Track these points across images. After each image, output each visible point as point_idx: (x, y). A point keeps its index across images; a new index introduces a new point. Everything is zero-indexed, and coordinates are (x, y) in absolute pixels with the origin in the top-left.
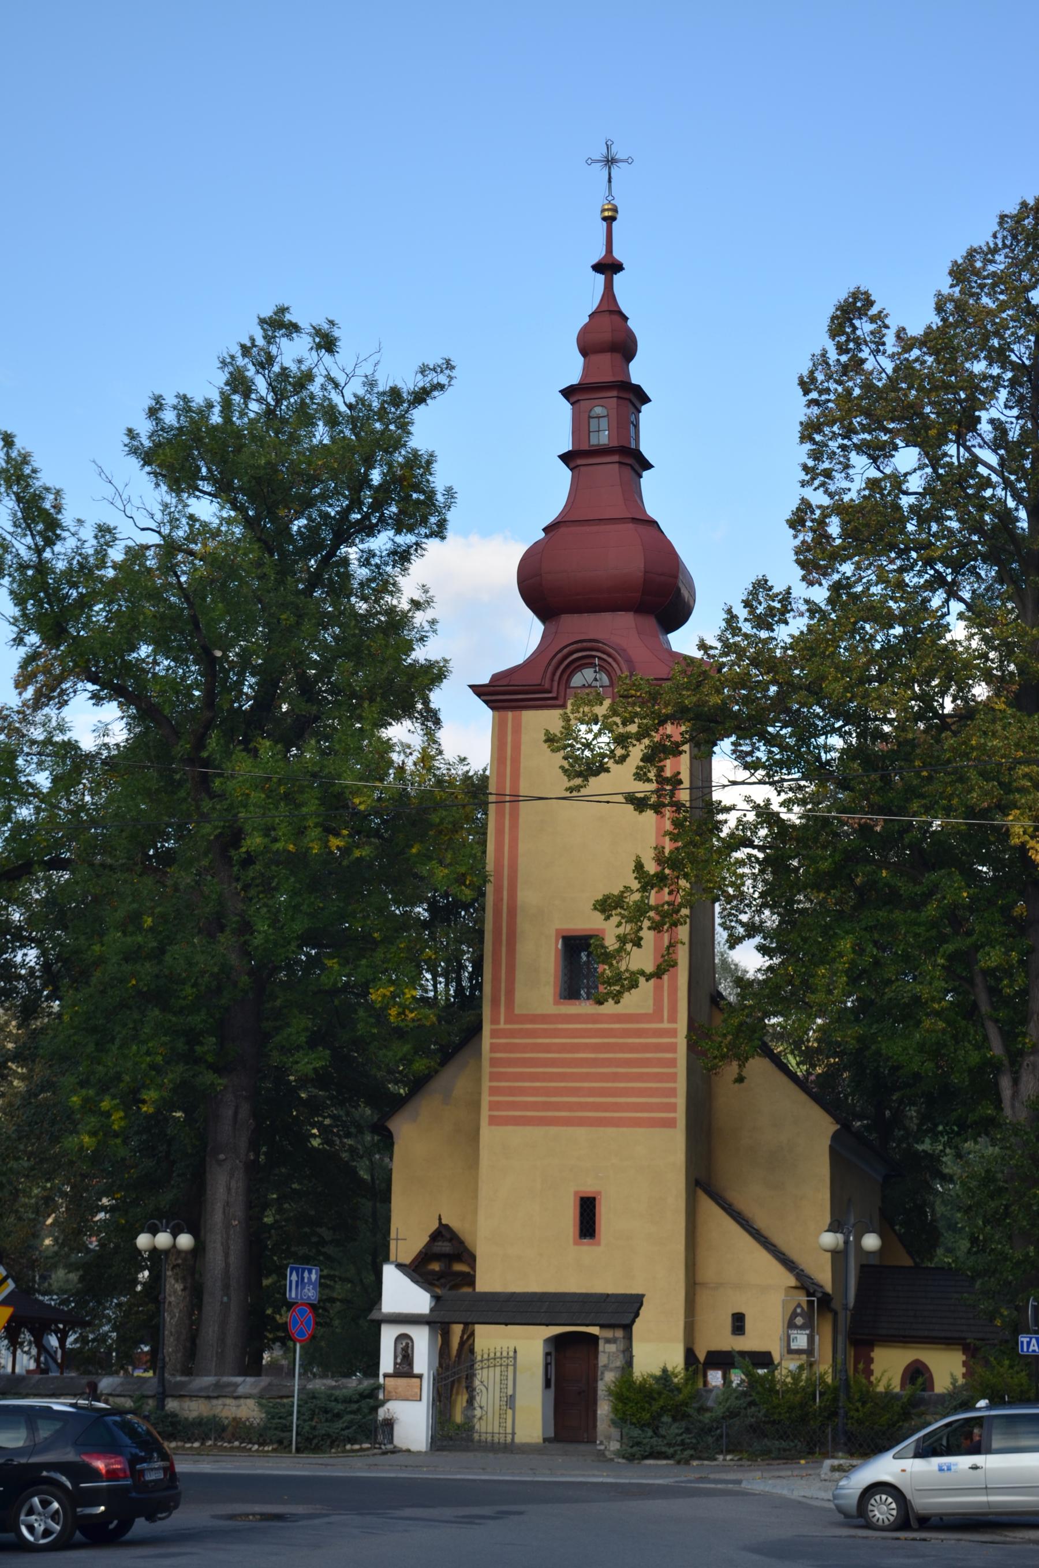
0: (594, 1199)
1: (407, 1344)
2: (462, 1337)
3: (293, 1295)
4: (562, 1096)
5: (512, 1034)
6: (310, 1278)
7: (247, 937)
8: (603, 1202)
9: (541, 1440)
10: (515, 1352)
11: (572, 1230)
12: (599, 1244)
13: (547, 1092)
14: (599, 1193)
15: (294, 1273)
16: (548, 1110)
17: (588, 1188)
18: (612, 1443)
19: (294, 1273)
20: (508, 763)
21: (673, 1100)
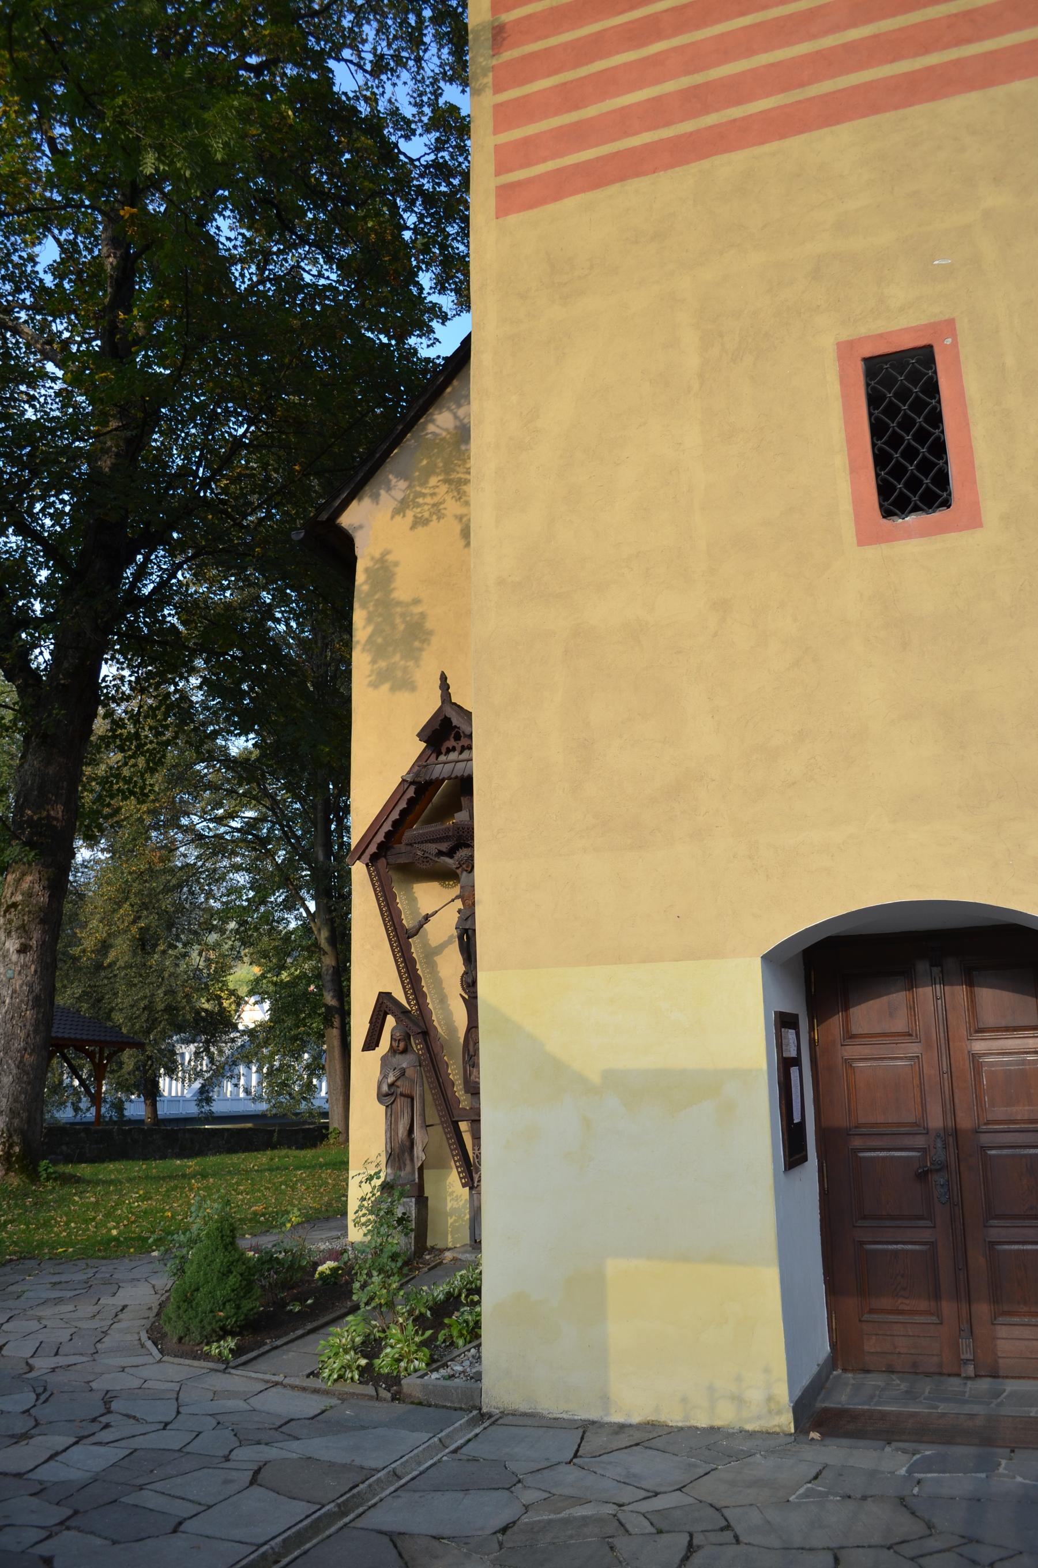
0: (925, 356)
4: (751, 52)
7: (411, 663)
8: (967, 351)
9: (786, 1421)
11: (844, 487)
14: (949, 326)
16: (707, 109)
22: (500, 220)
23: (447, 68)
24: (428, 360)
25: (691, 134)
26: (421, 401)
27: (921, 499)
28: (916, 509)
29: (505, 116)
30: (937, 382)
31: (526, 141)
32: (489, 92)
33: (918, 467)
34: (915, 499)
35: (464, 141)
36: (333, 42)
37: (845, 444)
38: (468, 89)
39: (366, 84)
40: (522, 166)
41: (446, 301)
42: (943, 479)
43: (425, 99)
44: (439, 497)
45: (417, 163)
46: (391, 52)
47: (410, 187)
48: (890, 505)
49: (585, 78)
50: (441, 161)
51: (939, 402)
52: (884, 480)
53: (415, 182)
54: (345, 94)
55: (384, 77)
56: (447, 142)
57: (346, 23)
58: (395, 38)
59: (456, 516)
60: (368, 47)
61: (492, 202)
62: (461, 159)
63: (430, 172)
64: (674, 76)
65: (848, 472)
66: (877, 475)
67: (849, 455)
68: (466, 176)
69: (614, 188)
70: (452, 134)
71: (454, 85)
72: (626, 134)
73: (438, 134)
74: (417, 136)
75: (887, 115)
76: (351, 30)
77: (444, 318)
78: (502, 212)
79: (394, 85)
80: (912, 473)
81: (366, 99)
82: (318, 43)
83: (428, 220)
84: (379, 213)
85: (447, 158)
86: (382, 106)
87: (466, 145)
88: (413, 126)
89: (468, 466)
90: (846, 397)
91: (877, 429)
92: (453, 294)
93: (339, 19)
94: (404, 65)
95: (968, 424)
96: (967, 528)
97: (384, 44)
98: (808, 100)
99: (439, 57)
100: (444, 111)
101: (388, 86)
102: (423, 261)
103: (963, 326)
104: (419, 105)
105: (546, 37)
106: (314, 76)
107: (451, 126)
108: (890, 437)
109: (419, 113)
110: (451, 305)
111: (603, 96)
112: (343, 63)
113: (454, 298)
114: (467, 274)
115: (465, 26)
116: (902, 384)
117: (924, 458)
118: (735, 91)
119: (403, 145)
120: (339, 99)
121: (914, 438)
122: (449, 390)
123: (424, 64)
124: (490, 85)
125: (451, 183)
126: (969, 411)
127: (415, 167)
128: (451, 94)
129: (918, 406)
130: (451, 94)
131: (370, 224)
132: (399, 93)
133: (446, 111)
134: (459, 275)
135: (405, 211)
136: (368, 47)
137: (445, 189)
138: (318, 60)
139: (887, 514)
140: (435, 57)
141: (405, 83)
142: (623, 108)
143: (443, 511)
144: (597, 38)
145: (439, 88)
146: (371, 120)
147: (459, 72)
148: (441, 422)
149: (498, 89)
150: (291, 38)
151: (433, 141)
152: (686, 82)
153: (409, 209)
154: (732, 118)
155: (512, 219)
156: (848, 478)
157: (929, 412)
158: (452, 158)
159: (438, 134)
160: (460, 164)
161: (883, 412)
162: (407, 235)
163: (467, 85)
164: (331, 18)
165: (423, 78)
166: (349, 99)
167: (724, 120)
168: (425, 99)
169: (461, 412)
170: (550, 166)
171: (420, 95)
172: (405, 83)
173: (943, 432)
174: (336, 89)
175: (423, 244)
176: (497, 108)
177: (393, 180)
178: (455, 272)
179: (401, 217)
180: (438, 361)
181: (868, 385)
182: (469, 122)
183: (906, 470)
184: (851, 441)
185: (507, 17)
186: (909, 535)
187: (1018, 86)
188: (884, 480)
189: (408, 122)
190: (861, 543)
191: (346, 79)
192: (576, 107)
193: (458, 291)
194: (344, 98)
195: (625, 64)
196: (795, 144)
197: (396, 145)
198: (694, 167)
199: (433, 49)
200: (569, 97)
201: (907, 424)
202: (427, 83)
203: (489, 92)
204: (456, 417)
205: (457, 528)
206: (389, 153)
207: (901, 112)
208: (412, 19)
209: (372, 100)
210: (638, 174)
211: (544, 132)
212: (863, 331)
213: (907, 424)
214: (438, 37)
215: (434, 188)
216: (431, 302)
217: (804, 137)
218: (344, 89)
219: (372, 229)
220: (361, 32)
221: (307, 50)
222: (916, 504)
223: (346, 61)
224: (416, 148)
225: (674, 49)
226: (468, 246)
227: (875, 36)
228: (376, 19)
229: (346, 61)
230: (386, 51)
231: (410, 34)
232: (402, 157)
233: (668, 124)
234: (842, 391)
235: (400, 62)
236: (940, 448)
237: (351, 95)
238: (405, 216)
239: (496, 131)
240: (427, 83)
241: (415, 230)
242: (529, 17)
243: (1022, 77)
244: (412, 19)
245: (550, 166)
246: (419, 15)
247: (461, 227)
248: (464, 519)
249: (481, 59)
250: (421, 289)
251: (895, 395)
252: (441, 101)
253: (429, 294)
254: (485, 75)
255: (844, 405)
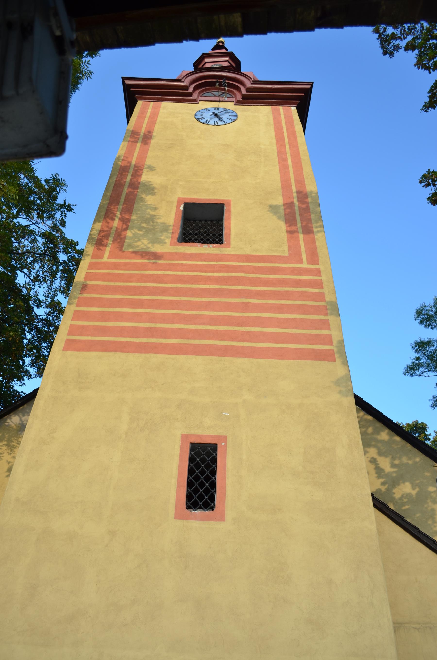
0: (214, 448)
4: (173, 322)
5: (116, 266)
13: (152, 318)
14: (224, 438)
16: (152, 337)
17: (205, 432)
21: (325, 332)
22: (64, 352)
23: (62, 288)
24: (17, 391)
25: (145, 343)
26: (8, 409)
27: (203, 504)
28: (200, 508)
29: (77, 315)
30: (217, 458)
31: (82, 327)
32: (74, 305)
33: (204, 491)
34: (201, 503)
35: (60, 315)
36: (22, 265)
37: (177, 475)
38: (68, 298)
39: (29, 283)
40: (78, 335)
41: (33, 371)
42: (212, 498)
43: (50, 295)
44: (2, 450)
45: (39, 317)
46: (43, 275)
47: (33, 325)
48: (191, 504)
49: (112, 312)
50: (48, 319)
51: (216, 466)
52: (190, 493)
53: (35, 323)
54: (19, 284)
55: (37, 283)
56: (53, 313)
57: (29, 260)
58: (46, 272)
59: (7, 461)
60: (34, 271)
61: (63, 344)
62: (56, 321)
63: (43, 322)
64: (144, 322)
65: (176, 487)
66: (187, 490)
67: (178, 480)
68: (56, 329)
69: (111, 354)
70: (56, 311)
71: (63, 295)
72: (122, 336)
73: (50, 310)
74: (42, 308)
75: (216, 357)
76: (30, 263)
77: (30, 377)
78: (65, 349)
79: (39, 287)
80: (201, 493)
81: (27, 288)
82: (16, 264)
83: (36, 339)
84: (16, 331)
85: (51, 319)
86: (32, 293)
87: (60, 317)
88: (42, 304)
89: (20, 439)
90: (181, 456)
91: (191, 472)
92: (36, 369)
93: (27, 258)
94: (46, 282)
95: (225, 478)
96: (219, 520)
97: (41, 272)
98: (189, 344)
99: (60, 284)
100: (55, 303)
101: (37, 287)
102: (28, 354)
103: (229, 439)
104: (47, 297)
105: (101, 294)
106: (10, 274)
107: (57, 309)
108: (195, 476)
109: (46, 299)
110: (34, 373)
111: (116, 320)
112: (22, 273)
113: (36, 371)
114: (45, 363)
115: (74, 278)
116: (203, 456)
117: (207, 488)
118: (164, 333)
119: (35, 309)
120: (16, 285)
121: (204, 478)
122: (21, 408)
123: (53, 284)
124: (76, 302)
125: (50, 328)
126: (227, 473)
127: (38, 318)
128: (60, 297)
129: (208, 466)
130: (60, 297)
131: (11, 334)
132: (41, 290)
133: (56, 303)
134: (41, 362)
135: (28, 332)
136: (34, 271)
137: (47, 330)
138: (14, 269)
139: (188, 507)
140: (58, 283)
141: (44, 288)
142: (123, 327)
143: (2, 457)
144: (120, 300)
145: (57, 293)
146: (26, 296)
147: (66, 291)
148: (14, 420)
149: (78, 305)
150: (6, 259)
151: (48, 311)
152: (147, 325)
153: (30, 332)
154: (161, 342)
155: (69, 353)
156: (176, 489)
157: (211, 482)
158: (53, 319)
159: (50, 310)
160: (55, 323)
161: (194, 465)
162: (25, 341)
163: (68, 296)
164: (24, 257)
165: (52, 288)
166: (20, 286)
167: (158, 342)
168: (50, 295)
169: (23, 418)
170: (89, 338)
171: (49, 294)
172: (44, 288)
173: (215, 479)
174: (16, 281)
175: (30, 348)
176: (76, 312)
177: (27, 320)
178: (40, 362)
179: (25, 335)
180: (21, 394)
181: (190, 453)
182: (64, 310)
183: (199, 491)
184: (180, 474)
185: (89, 283)
186: (195, 519)
187: (261, 361)
188: (190, 493)
189: (40, 302)
190: (176, 518)
191: (21, 279)
192: (105, 321)
193: (39, 368)
194: (18, 285)
195: (127, 312)
196: (182, 358)
197: (33, 308)
198: (143, 355)
199: (59, 280)
200: (104, 317)
201: (202, 472)
202: (53, 290)
203: (74, 305)
204: (21, 420)
205: (6, 467)
206: (29, 310)
207: (221, 358)
208: (54, 268)
209: (29, 290)
210: (122, 351)
211: (91, 326)
212: (192, 432)
213: (202, 472)
214: (62, 277)
215: (42, 327)
216: (26, 369)
217: (185, 356)
218: (19, 282)
219: (12, 336)
220: (33, 265)
221: (11, 265)
222: (200, 506)
223: (24, 273)
224: (40, 312)
225: (147, 313)
226: (49, 353)
227: (217, 330)
228: (41, 263)
229: (24, 273)
230: (41, 275)
231: (52, 272)
232: (33, 313)
233: (137, 337)
234: (180, 453)
235: (45, 280)
236: (213, 485)
237: (22, 285)
238: (27, 334)
239: (72, 320)
240: (53, 290)
241: (29, 341)
242: (97, 285)
243: (262, 358)
244: (54, 268)
245: (89, 338)
246: (57, 268)
247: (48, 345)
248: (11, 464)
249: (75, 293)
250: (24, 362)
251: (200, 460)
252: (56, 299)
253: (26, 366)
254: (75, 299)
255: (179, 459)
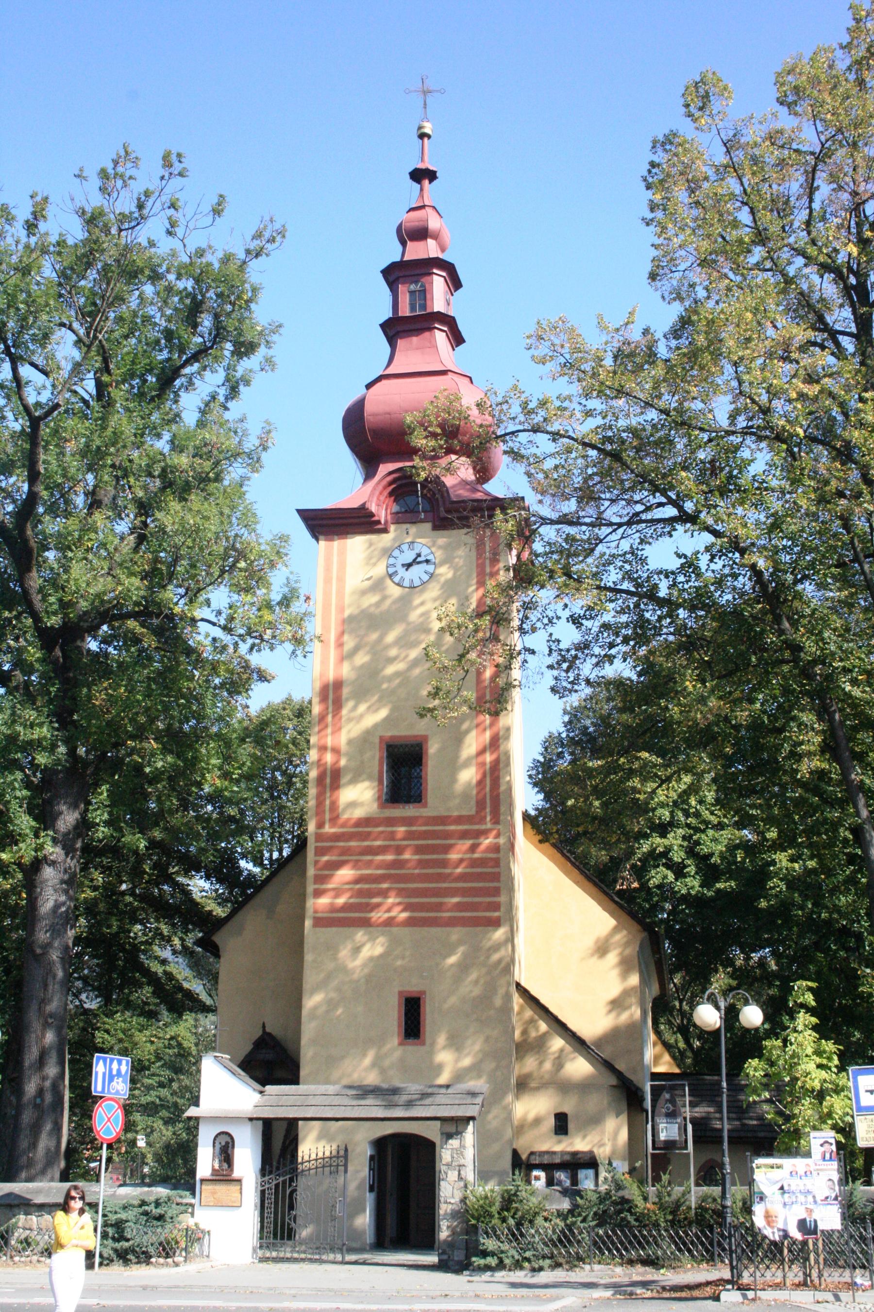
1: (227, 1143)
2: (284, 1143)
3: (99, 1088)
6: (119, 1071)
10: (346, 1150)
12: (424, 1044)
14: (424, 993)
15: (101, 1062)
17: (413, 986)
18: (456, 1253)
19: (101, 1062)
20: (334, 581)
